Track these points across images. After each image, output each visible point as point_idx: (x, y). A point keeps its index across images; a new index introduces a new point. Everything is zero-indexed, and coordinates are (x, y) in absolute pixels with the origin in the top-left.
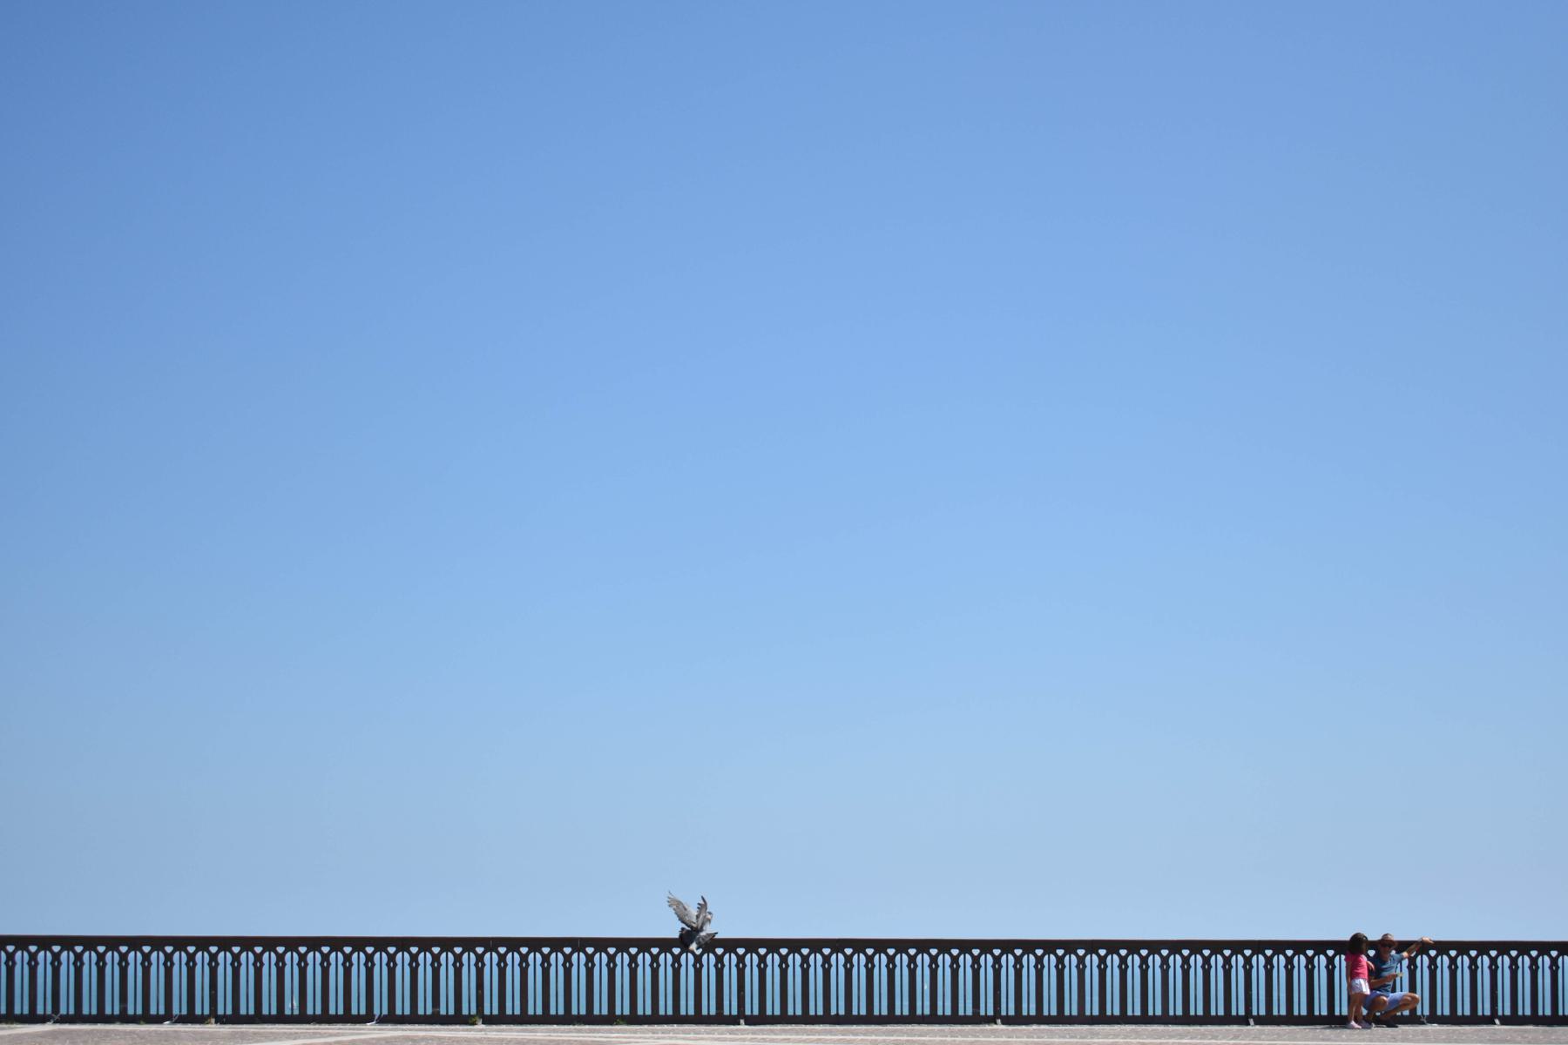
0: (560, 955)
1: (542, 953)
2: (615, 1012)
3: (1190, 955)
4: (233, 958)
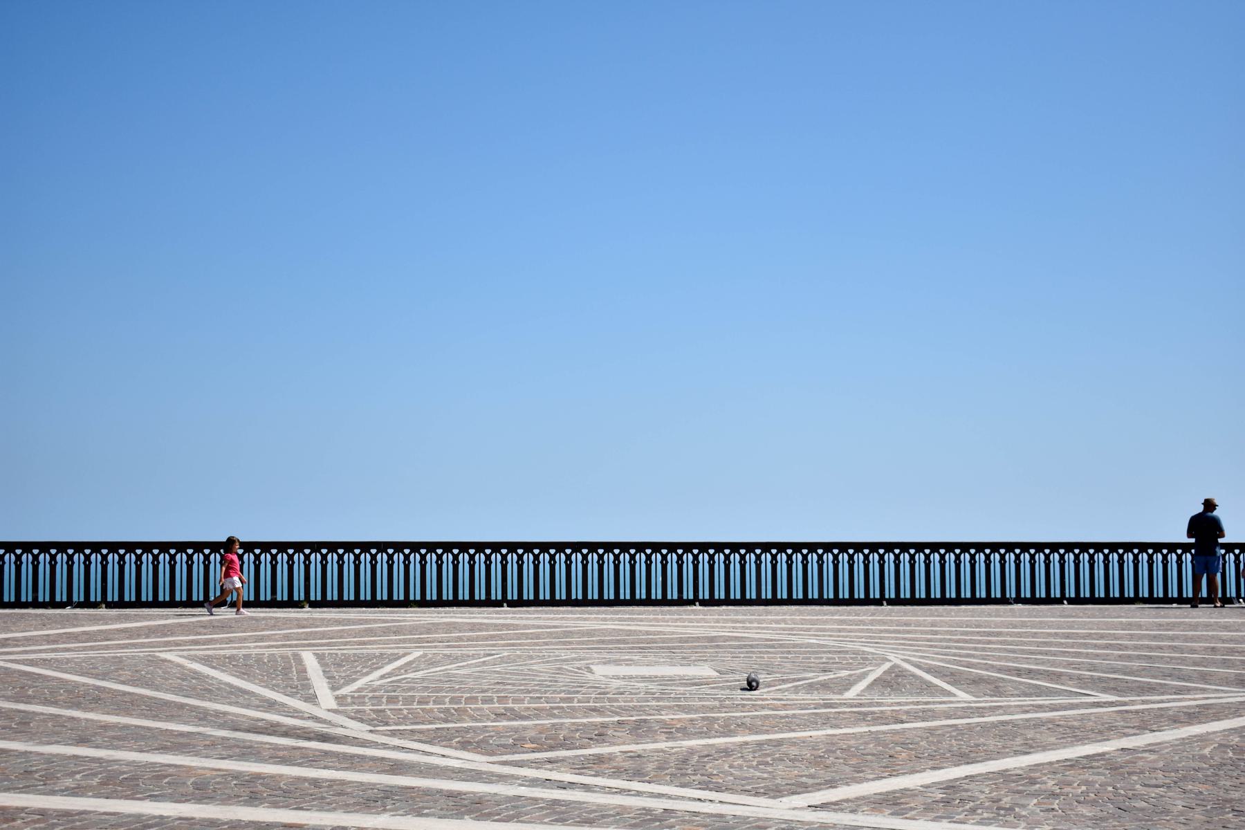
0: (268, 555)
1: (485, 554)
2: (141, 599)
3: (410, 554)
4: (880, 557)
